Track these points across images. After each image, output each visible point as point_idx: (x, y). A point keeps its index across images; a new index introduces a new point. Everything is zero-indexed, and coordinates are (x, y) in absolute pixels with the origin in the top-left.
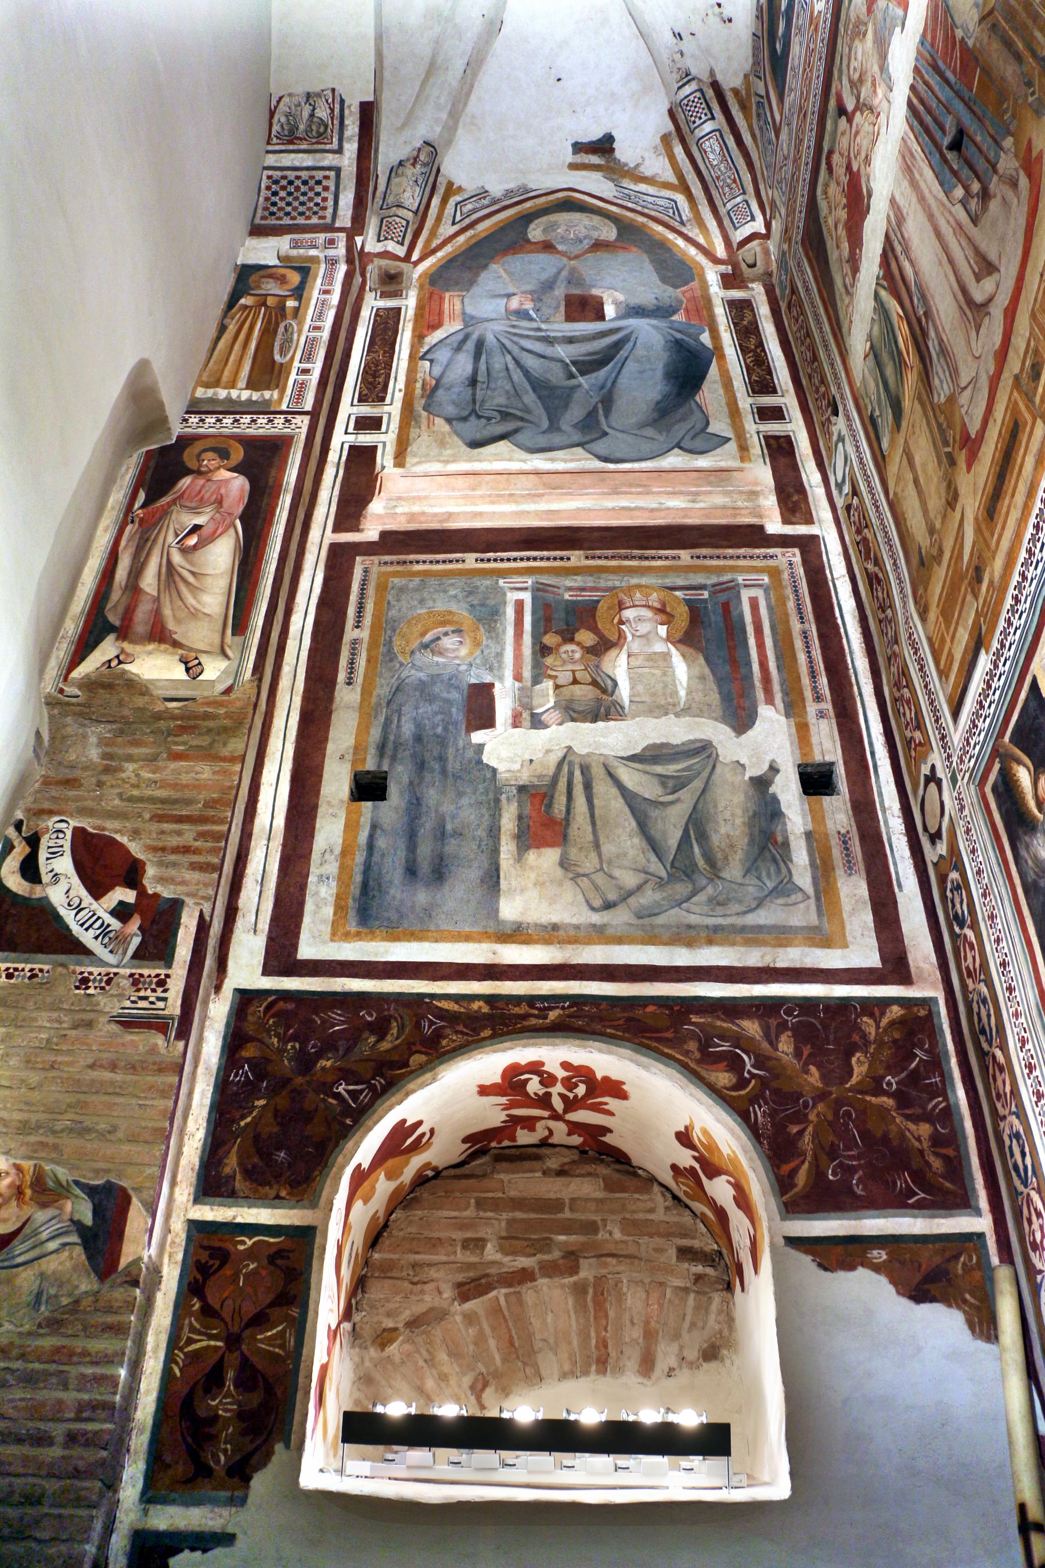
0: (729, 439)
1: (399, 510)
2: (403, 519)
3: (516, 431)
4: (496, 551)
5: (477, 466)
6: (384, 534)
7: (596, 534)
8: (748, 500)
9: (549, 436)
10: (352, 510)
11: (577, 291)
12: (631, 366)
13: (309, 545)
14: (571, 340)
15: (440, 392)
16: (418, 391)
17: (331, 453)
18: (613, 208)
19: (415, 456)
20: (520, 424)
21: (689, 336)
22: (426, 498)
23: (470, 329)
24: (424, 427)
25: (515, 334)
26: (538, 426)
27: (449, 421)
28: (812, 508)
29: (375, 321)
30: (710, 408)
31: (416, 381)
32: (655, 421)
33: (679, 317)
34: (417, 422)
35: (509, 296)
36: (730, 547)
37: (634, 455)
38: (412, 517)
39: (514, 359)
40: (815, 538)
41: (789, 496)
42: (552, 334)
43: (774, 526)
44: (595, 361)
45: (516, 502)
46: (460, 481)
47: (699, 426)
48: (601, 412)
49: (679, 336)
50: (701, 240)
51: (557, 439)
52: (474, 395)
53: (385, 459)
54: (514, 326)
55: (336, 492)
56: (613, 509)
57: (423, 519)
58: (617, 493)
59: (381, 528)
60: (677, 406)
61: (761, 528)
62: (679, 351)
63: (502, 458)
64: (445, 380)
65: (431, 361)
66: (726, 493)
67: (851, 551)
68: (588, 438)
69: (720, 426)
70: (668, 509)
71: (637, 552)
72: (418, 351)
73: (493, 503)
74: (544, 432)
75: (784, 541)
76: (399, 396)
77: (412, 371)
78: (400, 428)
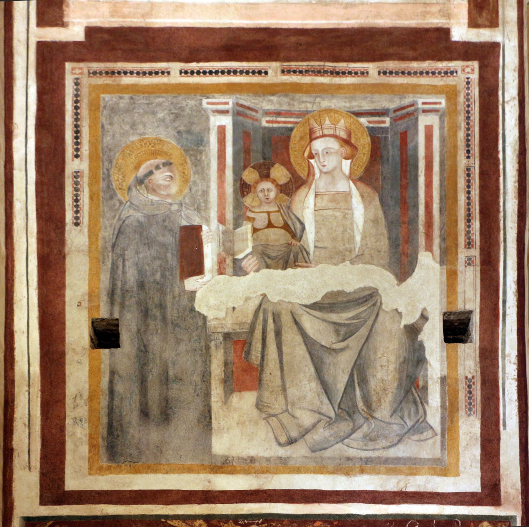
4: (198, 61)
6: (90, 31)
7: (293, 39)
36: (415, 59)
43: (461, 32)
57: (126, 10)
61: (445, 32)
71: (329, 65)
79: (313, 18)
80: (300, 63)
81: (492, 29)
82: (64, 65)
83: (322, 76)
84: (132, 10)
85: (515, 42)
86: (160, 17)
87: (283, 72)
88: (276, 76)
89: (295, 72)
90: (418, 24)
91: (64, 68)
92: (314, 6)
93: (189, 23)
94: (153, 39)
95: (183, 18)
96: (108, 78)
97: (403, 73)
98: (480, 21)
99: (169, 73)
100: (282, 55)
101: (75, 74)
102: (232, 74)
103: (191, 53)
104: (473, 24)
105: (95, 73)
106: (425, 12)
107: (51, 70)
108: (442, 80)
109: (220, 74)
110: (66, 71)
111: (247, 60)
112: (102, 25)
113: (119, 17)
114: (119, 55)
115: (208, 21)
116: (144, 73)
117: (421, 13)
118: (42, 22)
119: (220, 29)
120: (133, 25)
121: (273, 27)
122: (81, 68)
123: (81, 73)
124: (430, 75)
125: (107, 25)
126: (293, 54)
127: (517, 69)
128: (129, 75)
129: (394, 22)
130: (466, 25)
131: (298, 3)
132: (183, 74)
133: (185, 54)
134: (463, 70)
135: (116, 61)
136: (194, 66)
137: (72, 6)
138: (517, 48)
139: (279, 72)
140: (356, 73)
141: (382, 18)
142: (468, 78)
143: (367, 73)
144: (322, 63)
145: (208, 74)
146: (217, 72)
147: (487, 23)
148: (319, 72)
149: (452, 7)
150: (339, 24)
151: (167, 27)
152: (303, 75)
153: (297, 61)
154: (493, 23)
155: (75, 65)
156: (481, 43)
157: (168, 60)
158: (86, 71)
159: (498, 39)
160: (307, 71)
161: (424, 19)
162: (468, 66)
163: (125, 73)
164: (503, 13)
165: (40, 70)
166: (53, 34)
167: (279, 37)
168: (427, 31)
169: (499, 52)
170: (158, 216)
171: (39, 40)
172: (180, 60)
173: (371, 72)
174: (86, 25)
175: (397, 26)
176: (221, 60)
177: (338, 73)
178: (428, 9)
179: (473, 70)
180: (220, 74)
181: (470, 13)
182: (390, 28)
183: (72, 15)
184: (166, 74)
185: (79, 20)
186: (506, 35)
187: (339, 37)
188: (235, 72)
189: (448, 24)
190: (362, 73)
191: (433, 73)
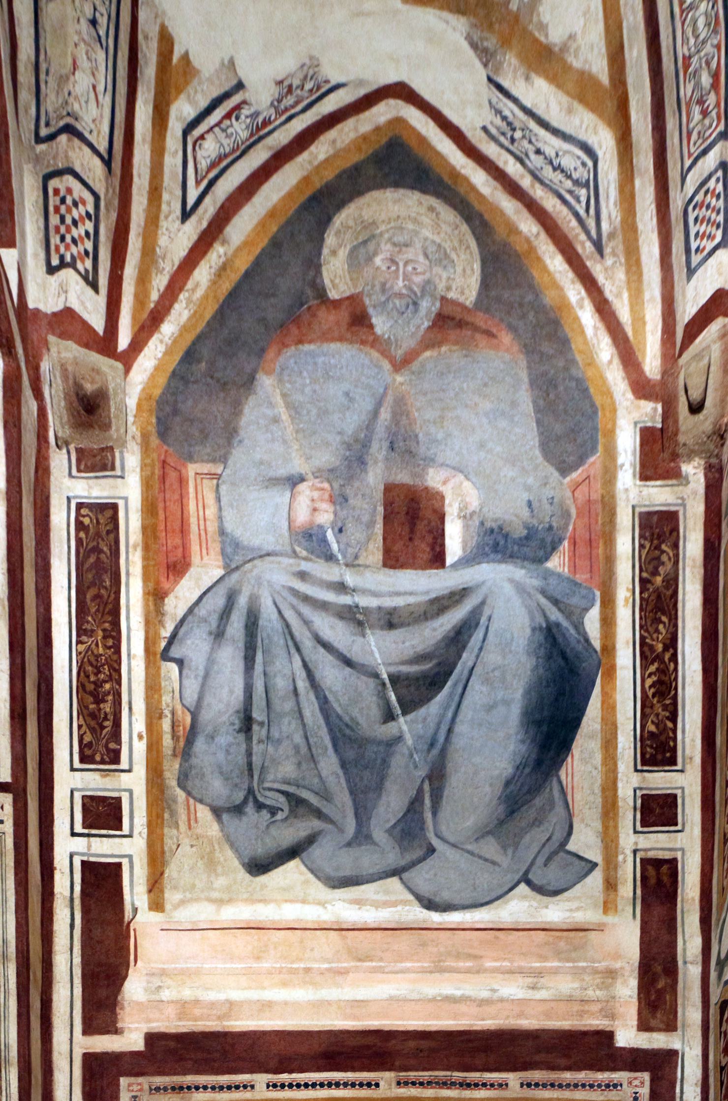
0: (595, 865)
1: (166, 995)
2: (171, 1011)
3: (311, 840)
4: (291, 1072)
5: (265, 913)
6: (152, 1039)
7: (412, 1044)
8: (602, 986)
9: (355, 852)
10: (103, 993)
11: (403, 477)
12: (477, 693)
13: (56, 1056)
14: (391, 620)
15: (200, 744)
16: (167, 741)
17: (57, 876)
18: (479, 178)
19: (175, 888)
20: (316, 824)
21: (568, 615)
22: (198, 972)
23: (235, 576)
24: (183, 826)
25: (306, 599)
26: (341, 831)
27: (217, 812)
28: (679, 1002)
29: (79, 541)
30: (578, 796)
31: (161, 716)
32: (501, 823)
33: (557, 563)
34: (173, 813)
35: (294, 481)
36: (568, 1068)
37: (466, 897)
38: (184, 1007)
39: (305, 665)
40: (672, 1055)
41: (654, 980)
42: (364, 601)
43: (627, 1036)
44: (424, 676)
45: (314, 984)
46: (242, 942)
47: (558, 836)
48: (427, 802)
49: (555, 615)
50: (624, 314)
51: (367, 859)
52: (249, 754)
53: (135, 891)
54: (303, 576)
55: (77, 960)
56: (434, 1000)
57: (197, 1012)
58: (442, 970)
59: (145, 1028)
60: (535, 790)
61: (608, 1036)
62: (549, 657)
63: (295, 895)
64: (206, 716)
65: (180, 663)
66: (577, 973)
67: (711, 1080)
68: (409, 857)
69: (585, 841)
70: (502, 1000)
71: (458, 1075)
72: (157, 635)
73: (284, 984)
74: (349, 844)
75: (635, 1060)
76: (140, 748)
77: (153, 687)
78: (150, 825)
79: (438, 1018)
80: (421, 1073)
81: (670, 1033)
82: (119, 1080)
83: (448, 1088)
84: (205, 1011)
85: (697, 1051)
86: (242, 1019)
87: (399, 1083)
88: (390, 1088)
89: (414, 1084)
90: (572, 1026)
91: (118, 1085)
92: (439, 1004)
93: (278, 1026)
94: (233, 1045)
95: (270, 1019)
96: (175, 1095)
97: (553, 1085)
98: (653, 1023)
99: (252, 1087)
100: (397, 1063)
101: (133, 1091)
102: (333, 1087)
103: (281, 1062)
104: (644, 1026)
105: (158, 1089)
106: (583, 1011)
107: (102, 1087)
108: (602, 1094)
109: (318, 1087)
110: (121, 1088)
111: (353, 1070)
112: (167, 1031)
113: (188, 1020)
114: (189, 1066)
115: (303, 1022)
116: (221, 1088)
117: (577, 1012)
118: (88, 1030)
119: (319, 1032)
120: (207, 1030)
121: (387, 1029)
122: (139, 1084)
123: (141, 1090)
124: (588, 1087)
125: (173, 1031)
126: (412, 1062)
127: (700, 1083)
128: (201, 1090)
129: (542, 1023)
130: (635, 1028)
131: (419, 1000)
132: (271, 1088)
133: (273, 1064)
134: (630, 1083)
135: (185, 1074)
136: (285, 1077)
137: (128, 1009)
138: (700, 1058)
139: (394, 1084)
140: (492, 1085)
141: (527, 1019)
142: (636, 1093)
143: (507, 1085)
144: (449, 1073)
145: (302, 1088)
146: (314, 1085)
147: (662, 1026)
148: (445, 1084)
149: (618, 1005)
150: (472, 1025)
151: (251, 1031)
152: (425, 1088)
153: (417, 1070)
154: (670, 1026)
155: (132, 1080)
156: (653, 1049)
157: (252, 1072)
158: (146, 1087)
159: (677, 1045)
160: (429, 1083)
161: (581, 1020)
162: (636, 1079)
163: (197, 1088)
164: (684, 1014)
165: (87, 1088)
166: (103, 1043)
167: (394, 1042)
168: (585, 1034)
169: (677, 1063)
170: (60, 434)
171: (85, 1051)
172: (267, 1071)
173: (511, 1084)
174: (146, 1031)
175: (546, 1028)
176: (319, 1070)
177: (469, 1085)
178: (586, 1008)
179: (642, 1083)
180: (318, 1087)
181: (640, 1013)
182: (537, 1030)
183: (127, 1019)
184: (249, 1088)
185: (136, 1025)
186: (686, 1042)
187: (470, 1041)
188: (337, 1085)
189: (612, 1026)
190: (500, 1085)
191: (591, 1086)
